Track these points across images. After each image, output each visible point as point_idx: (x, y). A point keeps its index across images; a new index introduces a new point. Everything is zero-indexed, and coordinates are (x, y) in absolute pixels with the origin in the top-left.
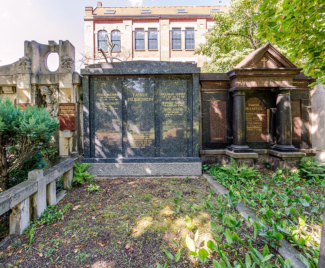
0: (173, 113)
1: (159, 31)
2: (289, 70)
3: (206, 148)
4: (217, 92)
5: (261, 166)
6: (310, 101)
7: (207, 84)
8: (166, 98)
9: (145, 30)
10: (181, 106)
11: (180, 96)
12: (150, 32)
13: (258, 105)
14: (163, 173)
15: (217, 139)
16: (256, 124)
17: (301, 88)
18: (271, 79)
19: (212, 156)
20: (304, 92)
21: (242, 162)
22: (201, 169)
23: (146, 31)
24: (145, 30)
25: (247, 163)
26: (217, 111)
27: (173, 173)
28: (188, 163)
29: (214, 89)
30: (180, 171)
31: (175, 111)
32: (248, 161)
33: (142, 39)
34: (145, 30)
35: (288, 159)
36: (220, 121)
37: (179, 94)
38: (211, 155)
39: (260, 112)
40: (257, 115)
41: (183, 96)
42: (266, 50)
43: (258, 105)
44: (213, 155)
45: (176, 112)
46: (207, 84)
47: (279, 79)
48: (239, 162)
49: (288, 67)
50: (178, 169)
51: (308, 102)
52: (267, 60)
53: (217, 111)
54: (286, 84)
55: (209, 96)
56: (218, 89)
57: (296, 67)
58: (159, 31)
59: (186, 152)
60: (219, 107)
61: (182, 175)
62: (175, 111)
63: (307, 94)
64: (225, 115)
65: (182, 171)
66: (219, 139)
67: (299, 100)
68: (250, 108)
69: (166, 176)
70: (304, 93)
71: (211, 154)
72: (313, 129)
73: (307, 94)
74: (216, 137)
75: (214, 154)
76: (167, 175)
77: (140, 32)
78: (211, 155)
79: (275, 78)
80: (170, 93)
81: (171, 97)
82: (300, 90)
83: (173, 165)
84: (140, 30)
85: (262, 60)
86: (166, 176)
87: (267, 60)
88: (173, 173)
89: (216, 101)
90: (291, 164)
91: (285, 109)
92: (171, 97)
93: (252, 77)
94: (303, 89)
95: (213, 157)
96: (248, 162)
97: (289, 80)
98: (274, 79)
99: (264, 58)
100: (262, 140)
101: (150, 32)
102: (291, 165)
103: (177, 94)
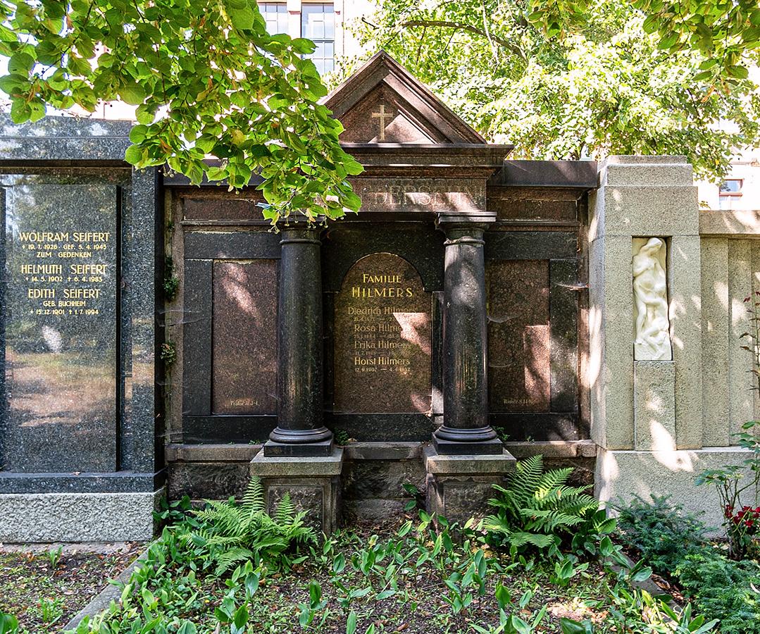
0: (63, 308)
1: (339, 13)
2: (457, 152)
3: (194, 439)
4: (241, 230)
5: (400, 504)
6: (584, 264)
7: (201, 200)
8: (37, 250)
9: (290, 7)
10: (92, 279)
11: (92, 243)
12: (310, 15)
13: (397, 279)
14: (7, 532)
15: (239, 403)
16: (388, 350)
17: (550, 217)
18: (405, 183)
19: (218, 468)
20: (559, 232)
21: (280, 493)
22: (151, 517)
23: (292, 12)
24: (288, 9)
25: (300, 495)
26: (243, 299)
27: (44, 531)
28: (102, 495)
29: (231, 218)
30: (71, 526)
31: (69, 299)
32: (304, 489)
33: (326, 41)
34: (290, 7)
35: (459, 478)
36: (251, 337)
37: (88, 236)
38: (215, 464)
39: (406, 305)
40: (392, 316)
41: (100, 243)
42: (379, 80)
43: (397, 279)
44: (221, 464)
45: (73, 304)
46: (201, 200)
47: (435, 183)
48: (272, 492)
49: (460, 141)
50: (63, 515)
51: (578, 270)
52: (391, 115)
53: (243, 299)
54: (462, 203)
55: (214, 246)
56: (245, 217)
57: (483, 143)
58: (339, 13)
59: (111, 454)
60: (248, 286)
61: (79, 539)
62: (69, 299)
63: (571, 239)
64: (271, 313)
65: (78, 525)
66: (232, 402)
67: (545, 260)
68: (367, 291)
69: (16, 543)
70: (561, 238)
71: (215, 461)
72: (590, 370)
73: (571, 239)
74: (238, 397)
75: (223, 461)
76: (19, 539)
77: (319, 16)
78: (215, 464)
79: (419, 179)
80: (54, 232)
81: (55, 247)
82: (544, 226)
83: (46, 500)
84: (274, 7)
85: (375, 115)
86: (16, 543)
87: (391, 115)
88: (44, 531)
89: (240, 263)
90: (462, 497)
91: (135, 321)
92: (55, 247)
93: (402, 175)
94: (557, 222)
95: (220, 473)
96: (303, 491)
97: (471, 190)
98: (419, 183)
99: (382, 107)
100: (410, 410)
101: (310, 15)
102: (463, 502)
103: (79, 237)
